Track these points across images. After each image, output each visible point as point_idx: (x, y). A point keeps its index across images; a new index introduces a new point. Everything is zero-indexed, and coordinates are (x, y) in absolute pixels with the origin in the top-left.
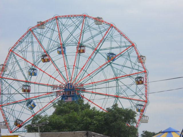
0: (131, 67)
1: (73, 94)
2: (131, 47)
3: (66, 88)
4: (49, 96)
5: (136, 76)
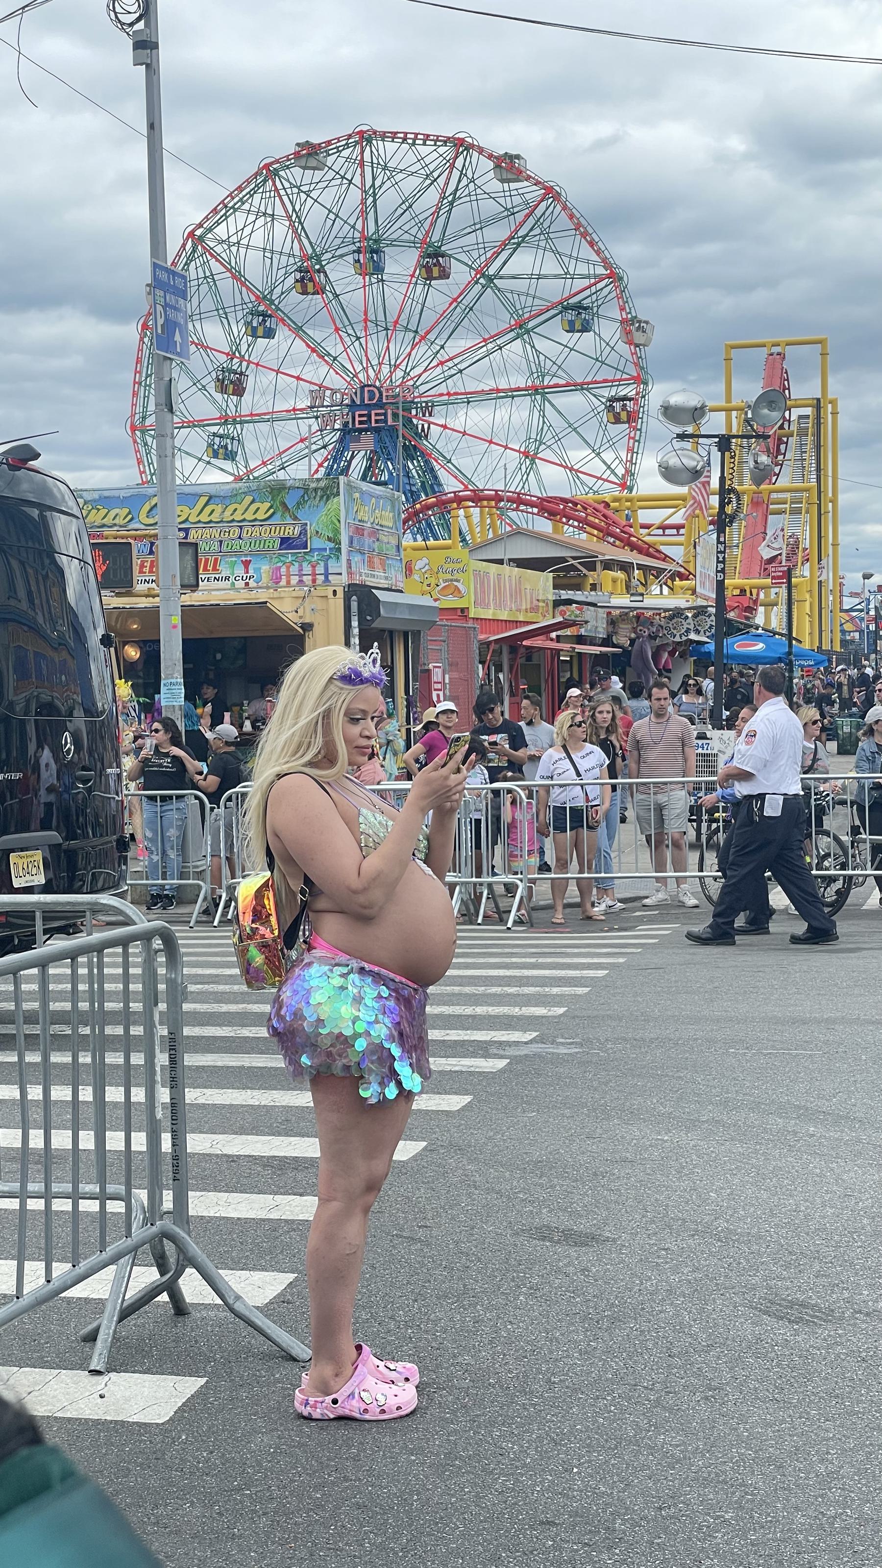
1: (377, 421)
3: (353, 401)
5: (606, 393)
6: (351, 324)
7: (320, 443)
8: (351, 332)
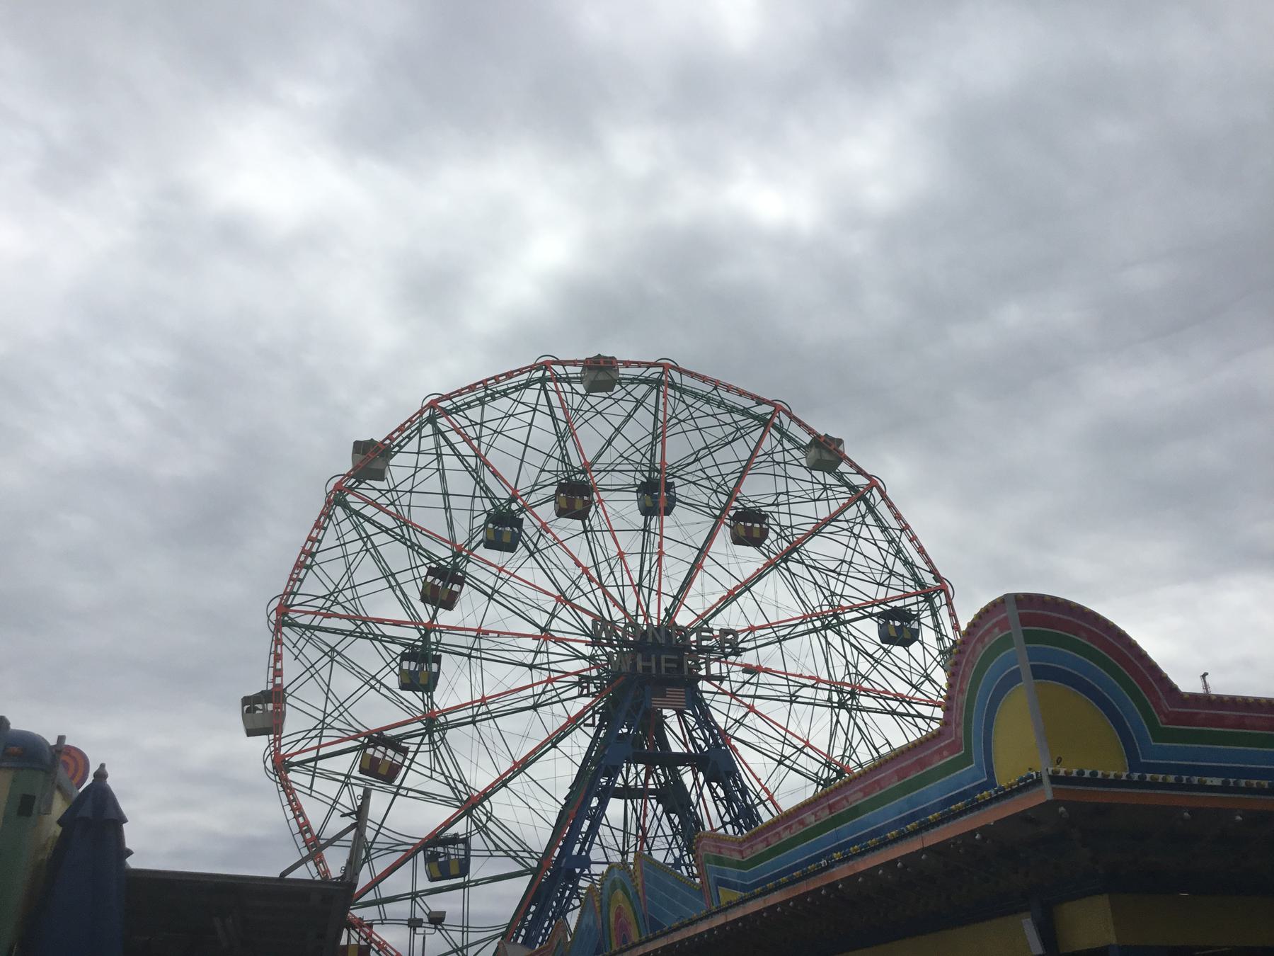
0: (533, 412)
2: (295, 759)
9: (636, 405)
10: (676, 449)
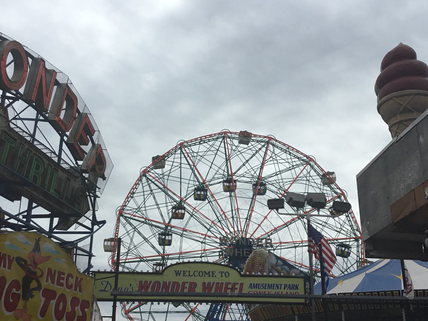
4: (232, 211)
6: (281, 249)
7: (235, 216)
8: (278, 248)
9: (256, 152)
10: (268, 170)
